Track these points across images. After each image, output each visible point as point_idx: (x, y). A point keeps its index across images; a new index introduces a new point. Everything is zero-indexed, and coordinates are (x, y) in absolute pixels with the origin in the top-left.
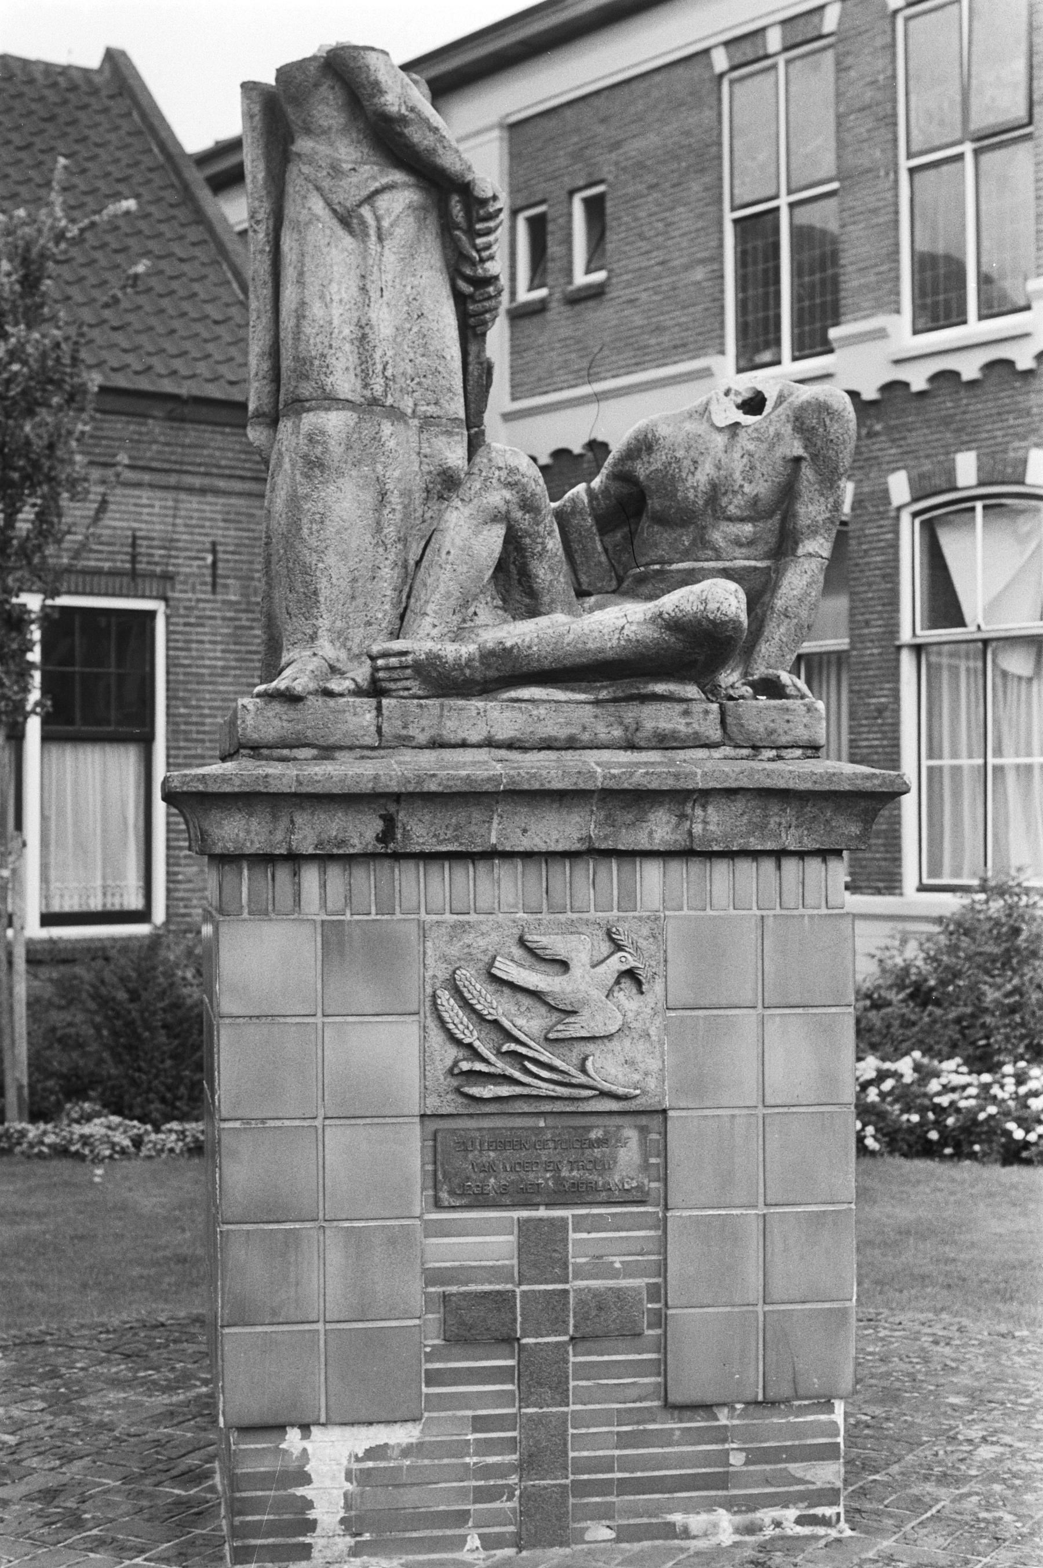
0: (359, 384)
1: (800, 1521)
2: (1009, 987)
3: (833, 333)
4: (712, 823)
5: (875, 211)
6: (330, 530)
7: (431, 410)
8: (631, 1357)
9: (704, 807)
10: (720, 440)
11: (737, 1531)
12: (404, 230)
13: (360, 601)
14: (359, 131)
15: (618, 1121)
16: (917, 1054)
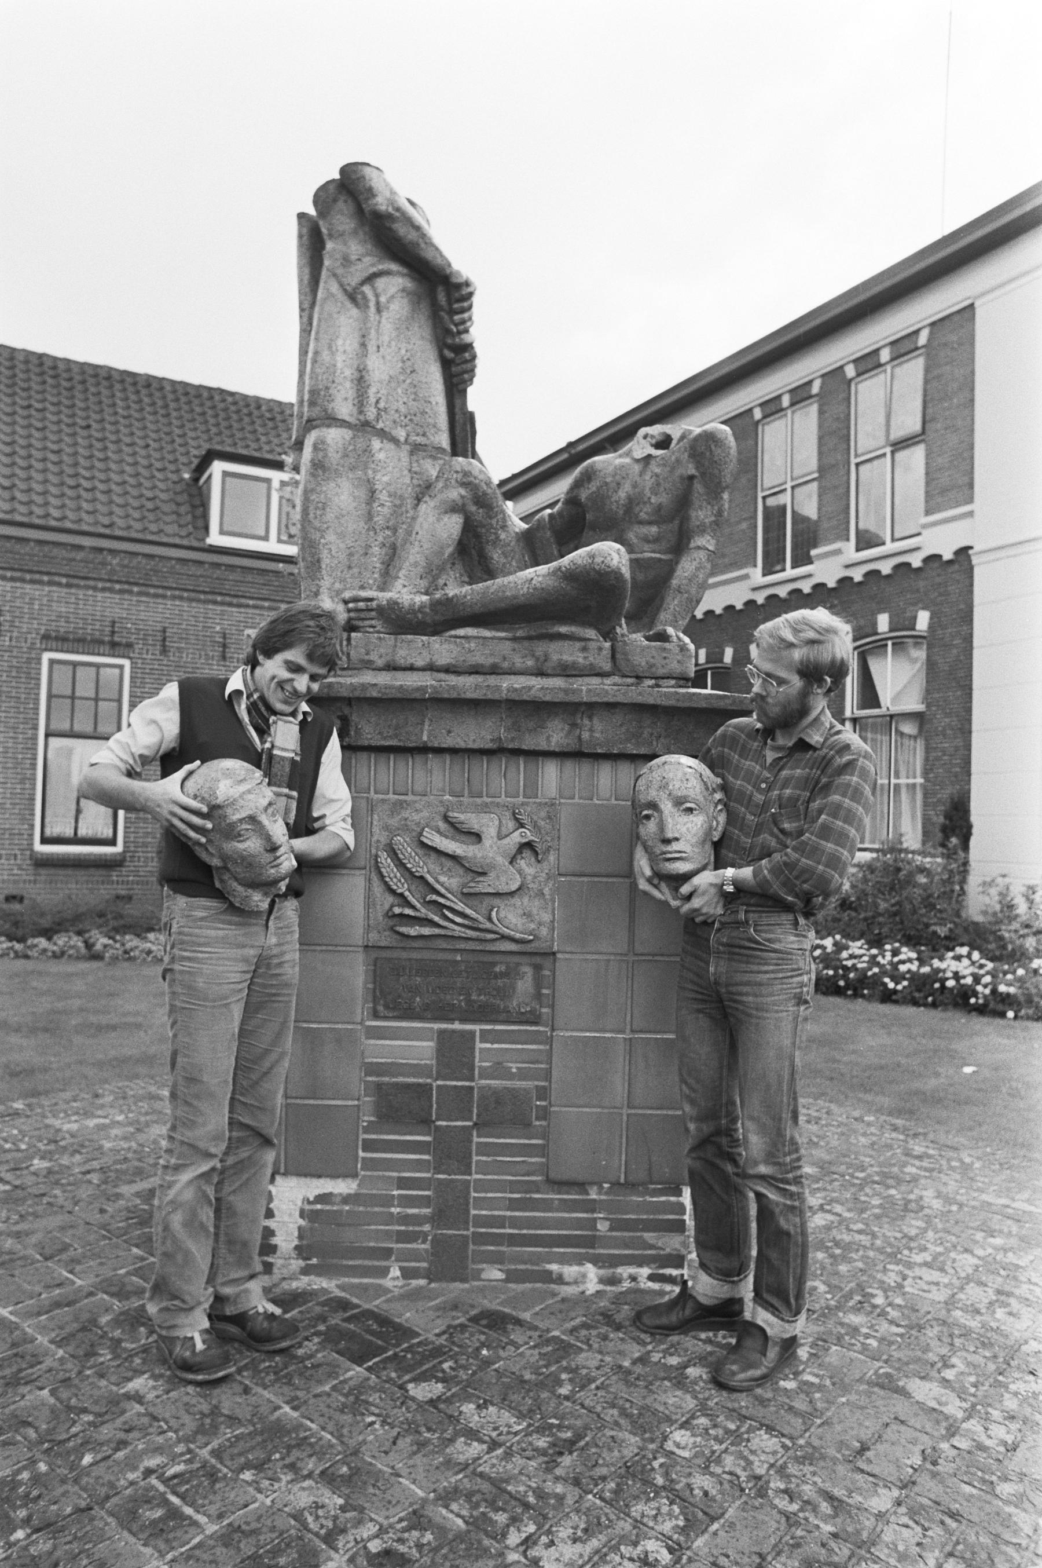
0: (355, 411)
1: (651, 1278)
2: (893, 901)
3: (813, 552)
4: (597, 732)
5: (836, 487)
6: (330, 516)
7: (419, 439)
8: (522, 1141)
9: (590, 718)
10: (637, 468)
11: (601, 1281)
12: (398, 308)
13: (355, 570)
14: (365, 233)
15: (516, 959)
16: (838, 937)
